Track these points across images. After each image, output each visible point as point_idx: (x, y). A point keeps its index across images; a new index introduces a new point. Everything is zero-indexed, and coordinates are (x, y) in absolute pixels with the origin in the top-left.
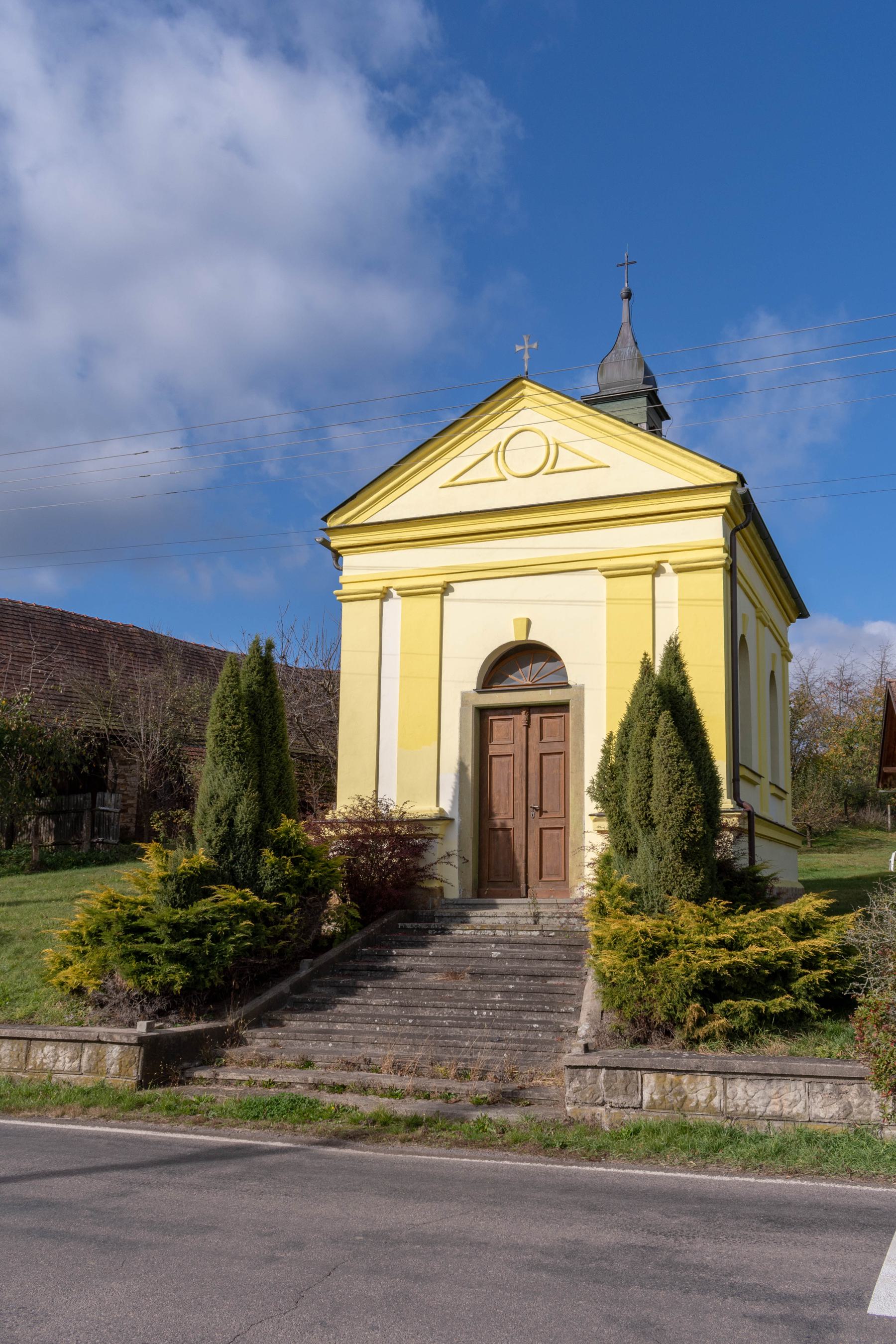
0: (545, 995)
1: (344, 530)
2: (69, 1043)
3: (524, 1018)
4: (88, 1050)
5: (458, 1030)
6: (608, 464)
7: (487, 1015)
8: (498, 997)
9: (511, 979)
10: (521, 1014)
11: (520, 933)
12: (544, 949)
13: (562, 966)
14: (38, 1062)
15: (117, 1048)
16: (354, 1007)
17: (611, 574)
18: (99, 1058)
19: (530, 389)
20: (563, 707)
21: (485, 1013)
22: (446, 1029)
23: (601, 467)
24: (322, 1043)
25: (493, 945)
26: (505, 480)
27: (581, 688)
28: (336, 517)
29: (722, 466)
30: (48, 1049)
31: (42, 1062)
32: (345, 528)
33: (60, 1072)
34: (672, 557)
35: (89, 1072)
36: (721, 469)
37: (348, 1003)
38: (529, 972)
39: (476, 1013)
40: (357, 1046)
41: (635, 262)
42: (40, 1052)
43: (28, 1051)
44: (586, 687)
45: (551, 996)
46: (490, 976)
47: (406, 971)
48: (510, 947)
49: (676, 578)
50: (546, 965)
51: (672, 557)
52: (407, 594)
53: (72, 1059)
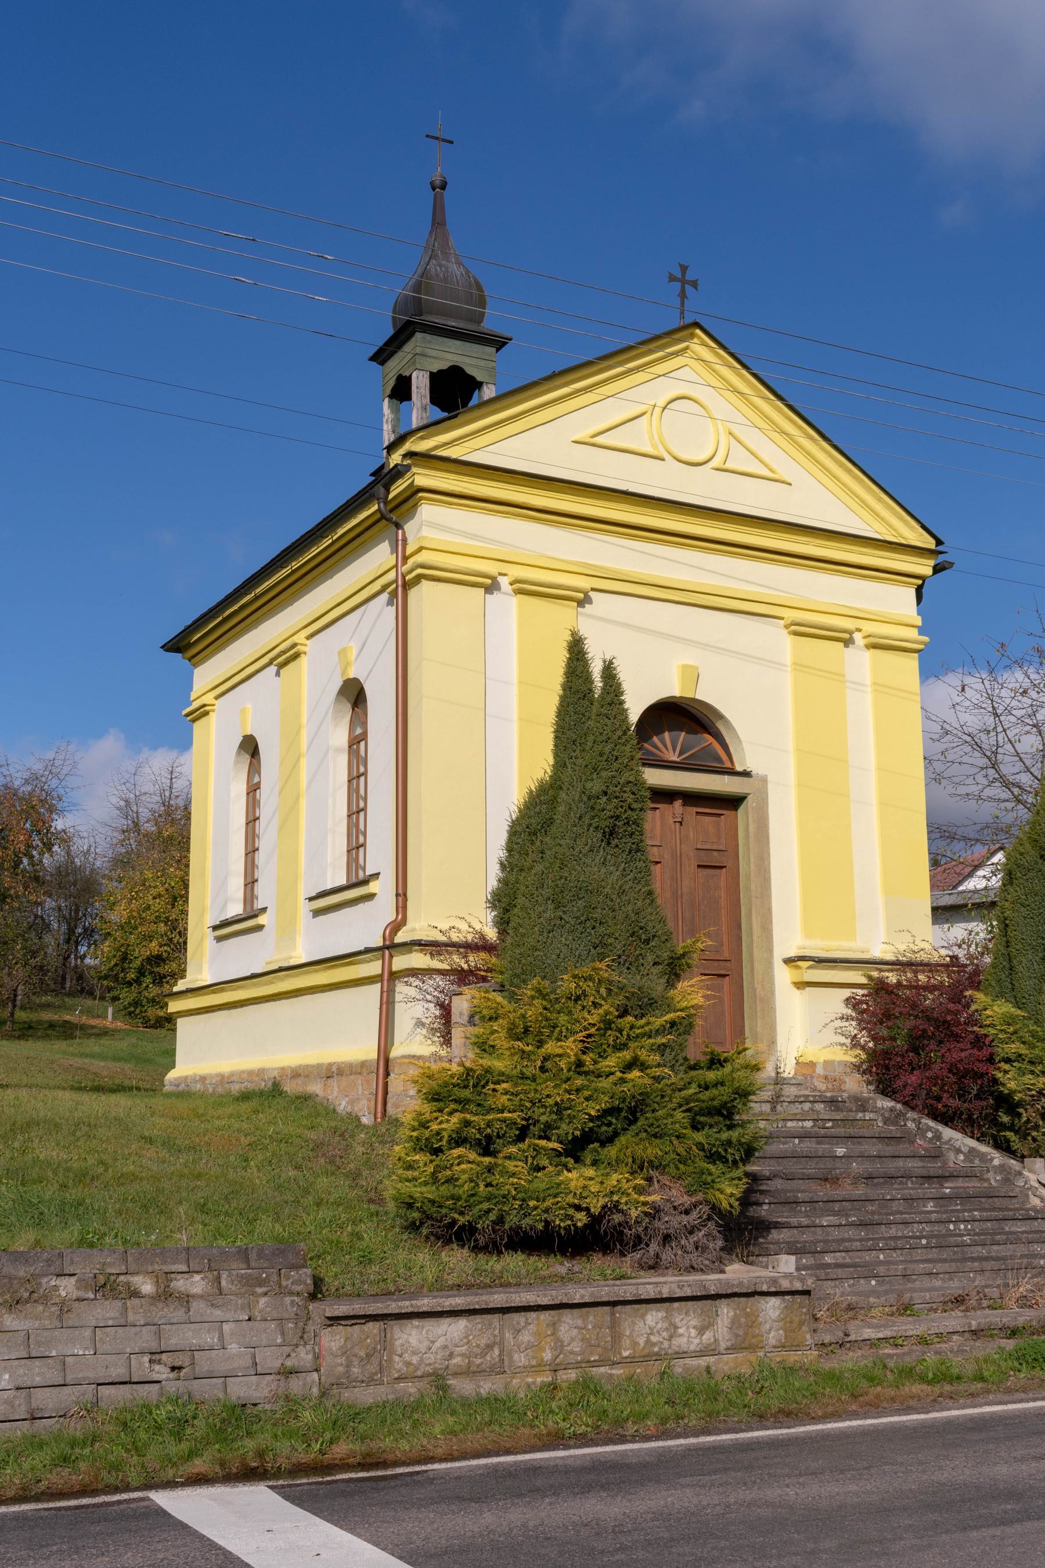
0: (983, 1200)
1: (451, 466)
2: (690, 1303)
3: (1007, 1229)
4: (726, 1311)
5: (979, 1248)
6: (790, 481)
7: (966, 1229)
8: (930, 1206)
9: (901, 1183)
10: (1003, 1224)
11: (790, 1124)
12: (859, 1143)
13: (920, 1164)
14: (642, 1341)
15: (774, 1301)
16: (795, 1231)
17: (801, 631)
18: (752, 1321)
19: (700, 346)
20: (734, 802)
21: (952, 1227)
22: (966, 1249)
23: (783, 482)
24: (862, 1281)
25: (797, 1141)
26: (663, 460)
27: (764, 780)
28: (422, 438)
29: (924, 527)
30: (654, 1317)
31: (648, 1341)
32: (427, 459)
33: (681, 1355)
34: (869, 627)
35: (732, 1349)
36: (921, 530)
37: (788, 1226)
38: (924, 1173)
39: (952, 1227)
40: (909, 1281)
41: (452, 142)
42: (642, 1324)
43: (614, 1325)
44: (769, 778)
45: (990, 1200)
46: (876, 1181)
47: (769, 1179)
48: (818, 1143)
49: (869, 655)
50: (900, 1163)
51: (869, 627)
52: (524, 589)
53: (701, 1330)
